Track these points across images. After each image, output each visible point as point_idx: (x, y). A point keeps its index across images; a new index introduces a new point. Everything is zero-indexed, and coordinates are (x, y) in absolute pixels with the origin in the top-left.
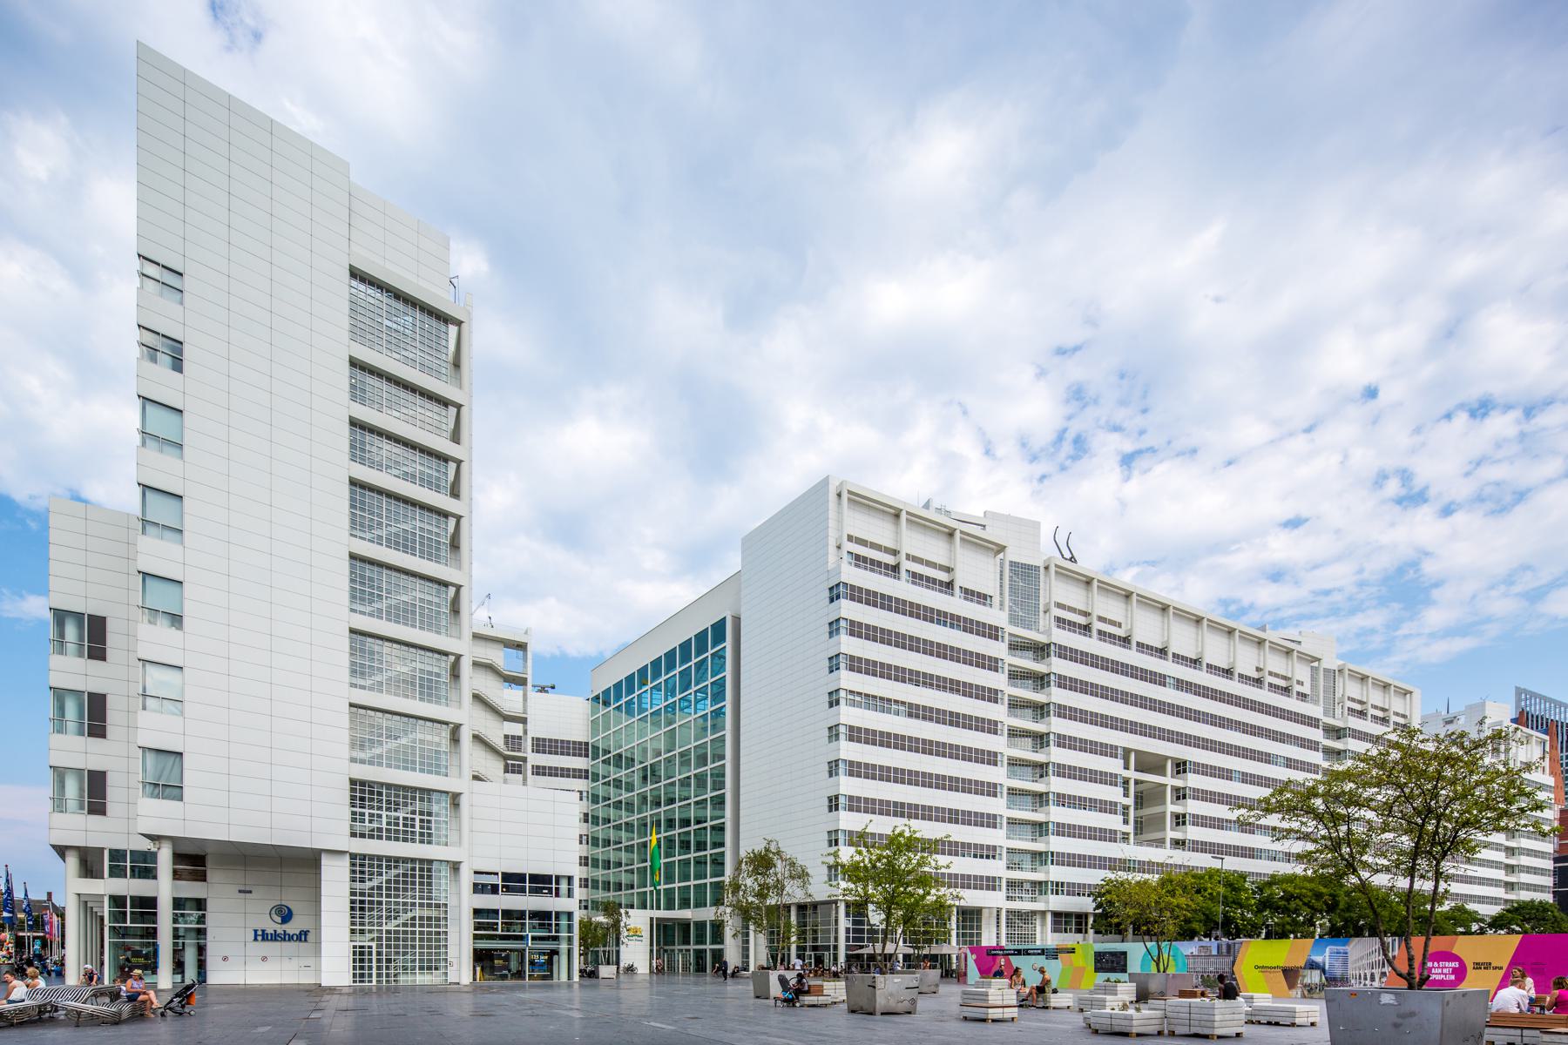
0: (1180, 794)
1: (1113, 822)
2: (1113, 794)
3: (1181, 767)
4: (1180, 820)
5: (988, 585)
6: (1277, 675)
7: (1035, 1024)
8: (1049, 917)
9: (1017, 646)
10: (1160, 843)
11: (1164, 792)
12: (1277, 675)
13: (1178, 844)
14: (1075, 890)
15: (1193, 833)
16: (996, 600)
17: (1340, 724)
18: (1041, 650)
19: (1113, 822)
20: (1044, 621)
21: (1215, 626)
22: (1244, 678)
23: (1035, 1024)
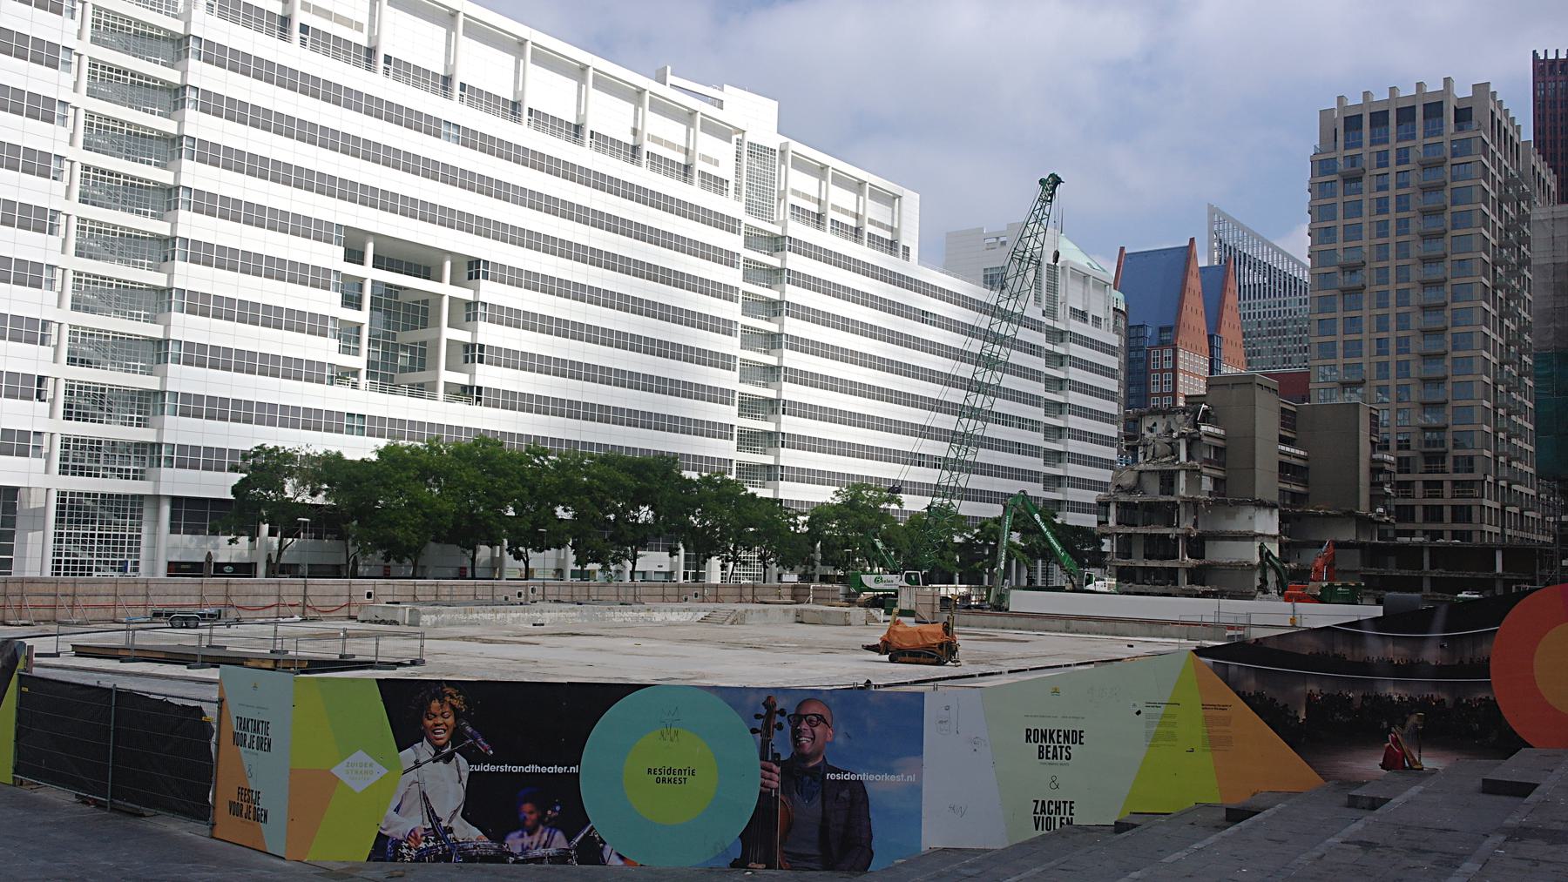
0: (468, 312)
1: (325, 350)
2: (327, 303)
3: (473, 269)
4: (472, 354)
5: (726, 170)
6: (881, 225)
7: (674, 617)
8: (166, 510)
9: (753, 239)
10: (421, 390)
11: (439, 306)
12: (881, 225)
13: (469, 393)
14: (211, 459)
15: (487, 376)
16: (732, 187)
17: (1060, 326)
18: (776, 244)
19: (325, 350)
20: (782, 212)
21: (1211, 355)
22: (839, 228)
23: (674, 617)
